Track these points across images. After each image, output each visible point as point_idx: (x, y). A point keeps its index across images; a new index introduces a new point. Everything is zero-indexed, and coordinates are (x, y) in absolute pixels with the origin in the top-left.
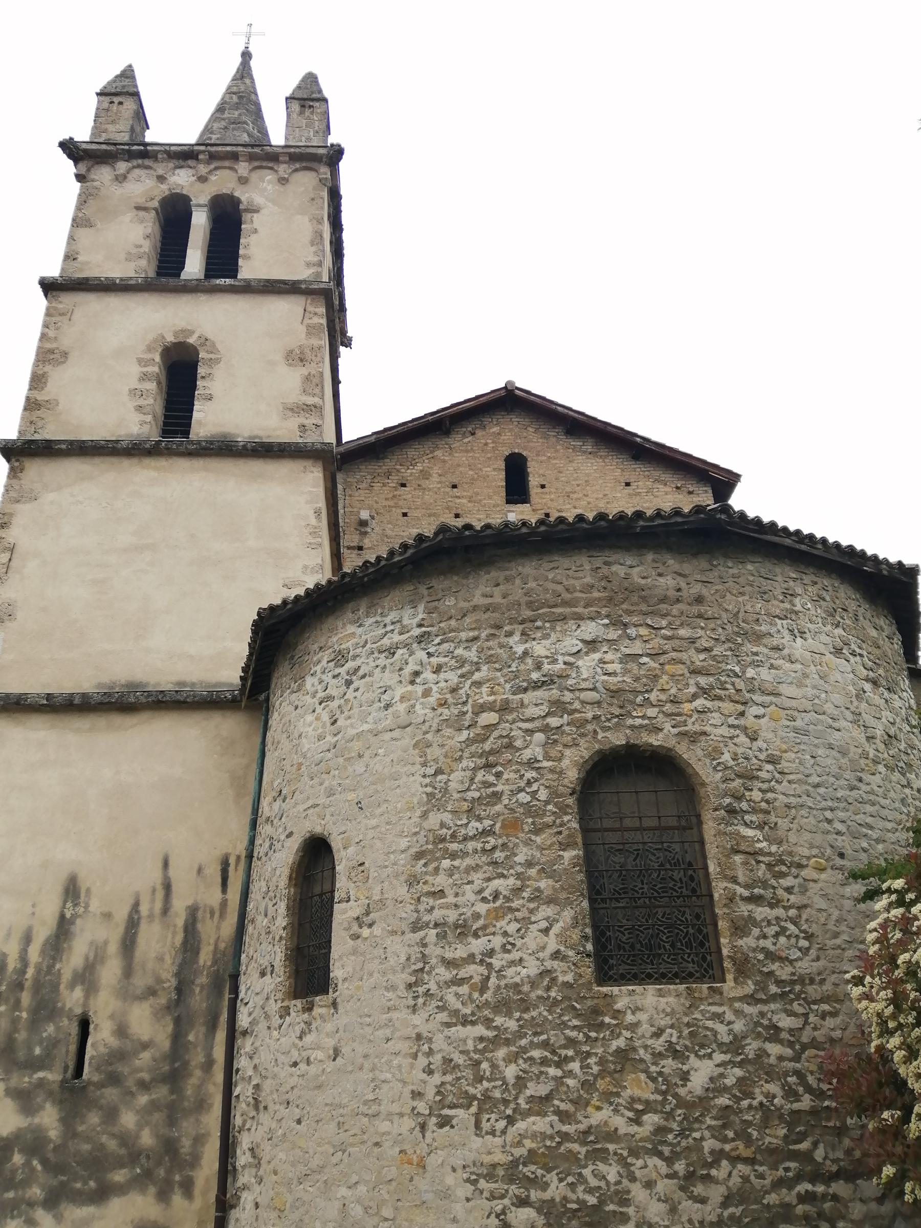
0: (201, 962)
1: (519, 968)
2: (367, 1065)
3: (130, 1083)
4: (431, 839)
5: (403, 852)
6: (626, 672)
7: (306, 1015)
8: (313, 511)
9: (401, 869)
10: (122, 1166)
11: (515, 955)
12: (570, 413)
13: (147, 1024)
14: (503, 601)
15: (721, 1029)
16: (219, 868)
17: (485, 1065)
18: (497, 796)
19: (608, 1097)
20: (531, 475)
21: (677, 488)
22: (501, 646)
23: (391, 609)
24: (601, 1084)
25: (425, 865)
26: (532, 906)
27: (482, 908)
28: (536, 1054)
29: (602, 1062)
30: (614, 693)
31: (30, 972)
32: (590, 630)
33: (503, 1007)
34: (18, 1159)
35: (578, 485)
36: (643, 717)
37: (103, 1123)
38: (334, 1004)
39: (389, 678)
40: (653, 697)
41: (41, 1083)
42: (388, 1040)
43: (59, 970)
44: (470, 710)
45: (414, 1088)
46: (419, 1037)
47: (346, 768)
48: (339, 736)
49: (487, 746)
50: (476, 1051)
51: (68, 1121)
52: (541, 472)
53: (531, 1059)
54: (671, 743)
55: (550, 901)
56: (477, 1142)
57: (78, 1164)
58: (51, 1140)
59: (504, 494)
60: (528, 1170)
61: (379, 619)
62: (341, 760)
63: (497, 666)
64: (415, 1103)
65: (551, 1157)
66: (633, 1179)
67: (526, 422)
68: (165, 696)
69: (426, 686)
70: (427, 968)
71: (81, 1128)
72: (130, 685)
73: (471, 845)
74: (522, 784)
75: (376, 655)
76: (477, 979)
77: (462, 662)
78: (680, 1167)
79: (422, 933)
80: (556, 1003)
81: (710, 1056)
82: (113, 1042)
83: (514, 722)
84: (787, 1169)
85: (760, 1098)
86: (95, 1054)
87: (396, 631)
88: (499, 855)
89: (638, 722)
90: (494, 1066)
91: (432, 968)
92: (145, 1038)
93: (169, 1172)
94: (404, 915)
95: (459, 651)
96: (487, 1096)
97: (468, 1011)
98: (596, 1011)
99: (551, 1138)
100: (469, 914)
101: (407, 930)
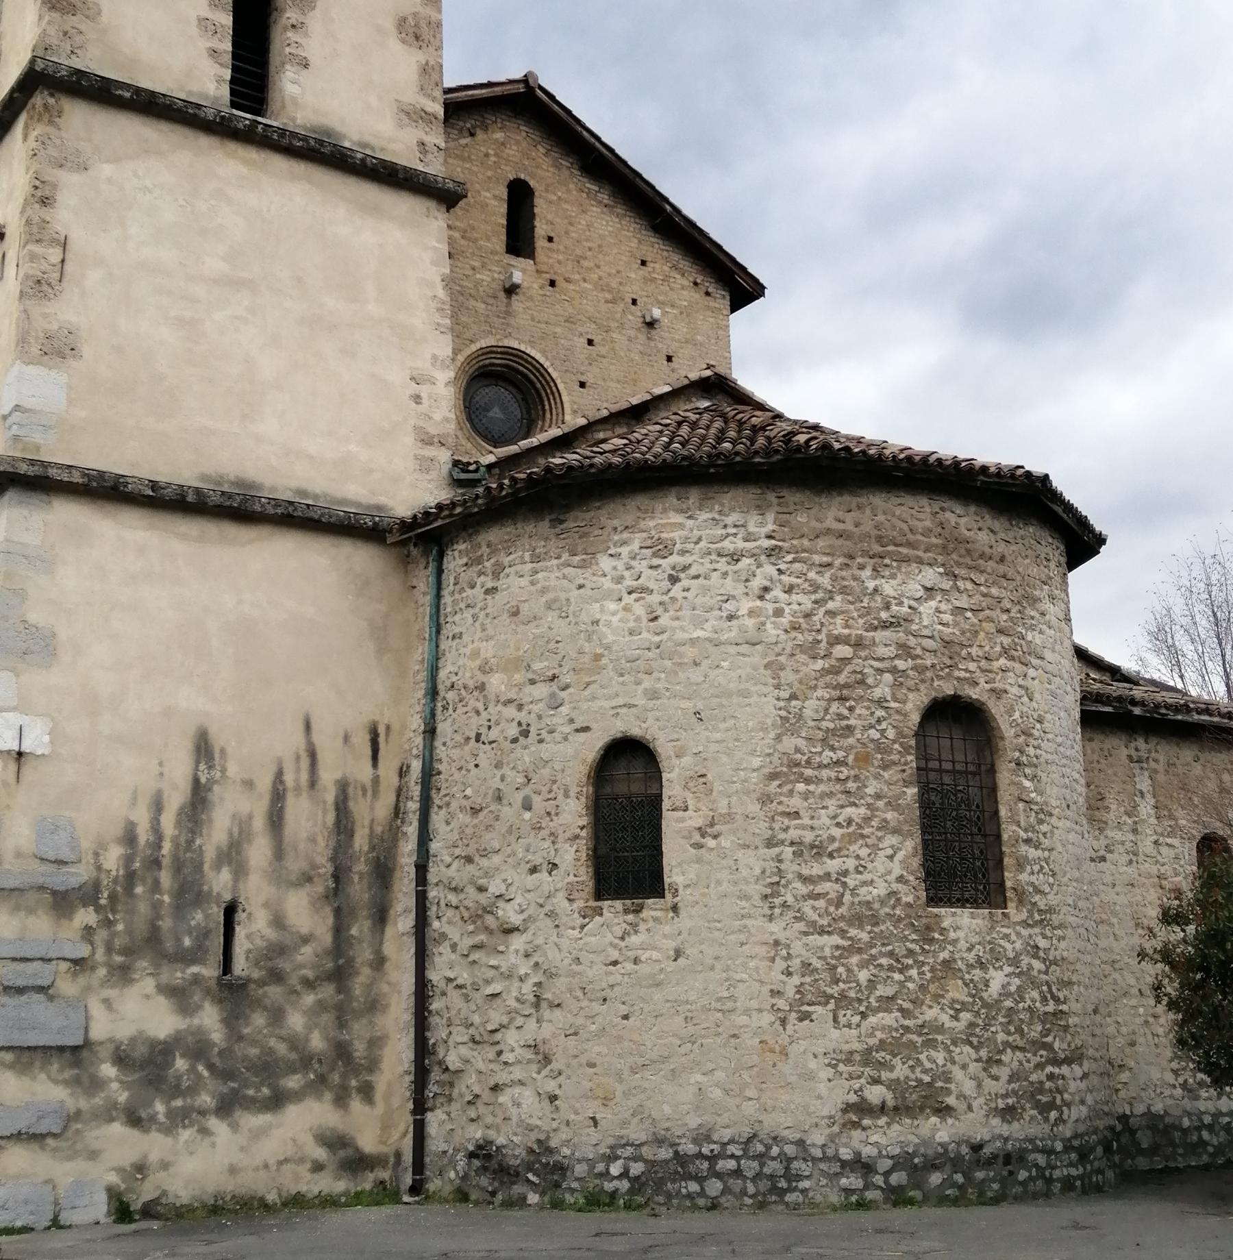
0: (357, 846)
1: (871, 888)
2: (718, 966)
3: (294, 981)
4: (785, 761)
5: (754, 770)
6: (956, 624)
7: (630, 917)
8: (439, 279)
9: (752, 787)
10: (295, 1072)
11: (866, 877)
12: (597, 144)
13: (305, 914)
14: (855, 530)
15: (1008, 946)
16: (368, 737)
17: (841, 970)
18: (850, 729)
19: (937, 997)
20: (537, 219)
21: (696, 284)
22: (855, 579)
23: (732, 509)
24: (932, 988)
25: (780, 786)
26: (880, 834)
27: (837, 832)
28: (884, 961)
29: (932, 970)
30: (947, 643)
31: (167, 847)
32: (930, 576)
33: (857, 920)
34: (181, 1064)
35: (590, 249)
36: (966, 670)
37: (269, 1025)
38: (675, 908)
39: (730, 586)
40: (974, 651)
41: (196, 980)
42: (742, 944)
43: (200, 847)
44: (825, 640)
45: (773, 987)
46: (777, 943)
47: (676, 673)
48: (664, 637)
49: (842, 679)
50: (833, 957)
51: (232, 1020)
52: (549, 217)
53: (880, 965)
54: (984, 698)
55: (895, 831)
56: (835, 1034)
57: (248, 1070)
58: (215, 1044)
59: (504, 237)
60: (879, 1056)
61: (717, 517)
62: (668, 663)
63: (850, 598)
64: (774, 1001)
65: (895, 1046)
66: (954, 1063)
67: (536, 136)
68: (295, 509)
69: (777, 605)
70: (783, 882)
71: (246, 1031)
72: (240, 483)
73: (825, 773)
74: (873, 721)
75: (714, 557)
76: (833, 895)
77: (816, 588)
78: (983, 1053)
79: (777, 850)
80: (900, 920)
81: (1001, 968)
82: (271, 934)
83: (866, 659)
84: (1041, 1056)
85: (1029, 1002)
86: (251, 947)
87: (740, 536)
88: (851, 785)
89: (962, 674)
90: (849, 970)
91: (789, 882)
92: (305, 930)
93: (344, 1076)
94: (757, 831)
95: (812, 575)
96: (843, 996)
97: (826, 923)
98: (928, 928)
99: (897, 1030)
100: (825, 836)
101: (761, 846)
